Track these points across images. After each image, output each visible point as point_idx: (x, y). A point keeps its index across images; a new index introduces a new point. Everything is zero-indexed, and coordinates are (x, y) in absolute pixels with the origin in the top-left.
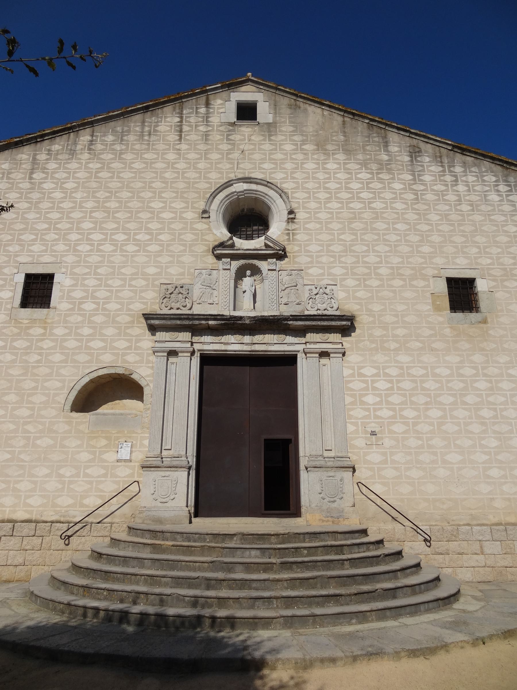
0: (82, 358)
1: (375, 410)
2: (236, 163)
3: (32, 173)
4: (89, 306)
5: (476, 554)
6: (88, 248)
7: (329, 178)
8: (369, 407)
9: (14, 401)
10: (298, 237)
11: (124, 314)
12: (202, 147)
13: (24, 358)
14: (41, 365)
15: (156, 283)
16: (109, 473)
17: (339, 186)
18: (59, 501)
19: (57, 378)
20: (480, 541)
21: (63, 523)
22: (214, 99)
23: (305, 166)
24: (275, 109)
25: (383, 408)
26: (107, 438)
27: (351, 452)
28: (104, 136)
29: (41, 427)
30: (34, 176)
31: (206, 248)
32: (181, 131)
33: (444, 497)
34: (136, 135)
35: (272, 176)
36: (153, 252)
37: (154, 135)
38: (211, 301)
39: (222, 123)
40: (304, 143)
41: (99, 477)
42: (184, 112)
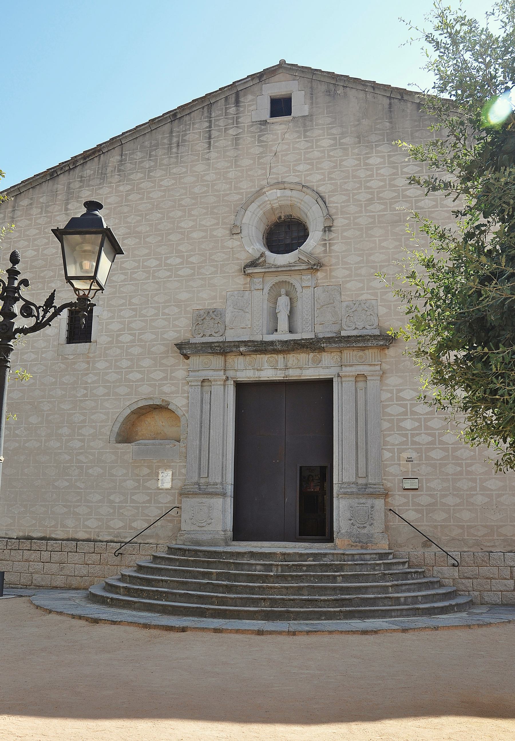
0: (122, 390)
1: (413, 435)
2: (268, 168)
3: (67, 204)
4: (126, 338)
5: (506, 579)
6: (122, 277)
7: (372, 176)
8: (407, 432)
9: (67, 433)
10: (335, 248)
11: (159, 344)
12: (231, 153)
13: (72, 392)
14: (87, 398)
15: (188, 309)
16: (153, 499)
17: (383, 183)
18: (111, 523)
19: (101, 411)
20: (511, 567)
21: (116, 543)
22: (245, 95)
23: (344, 163)
24: (312, 98)
25: (422, 433)
26: (149, 467)
27: (385, 479)
28: (133, 153)
29: (91, 457)
30: (69, 206)
31: (237, 267)
32: (210, 138)
33: (480, 524)
34: (164, 148)
35: (308, 178)
36: (184, 276)
37: (182, 145)
38: (243, 325)
39: (253, 122)
40: (343, 135)
41: (144, 503)
42: (213, 115)
